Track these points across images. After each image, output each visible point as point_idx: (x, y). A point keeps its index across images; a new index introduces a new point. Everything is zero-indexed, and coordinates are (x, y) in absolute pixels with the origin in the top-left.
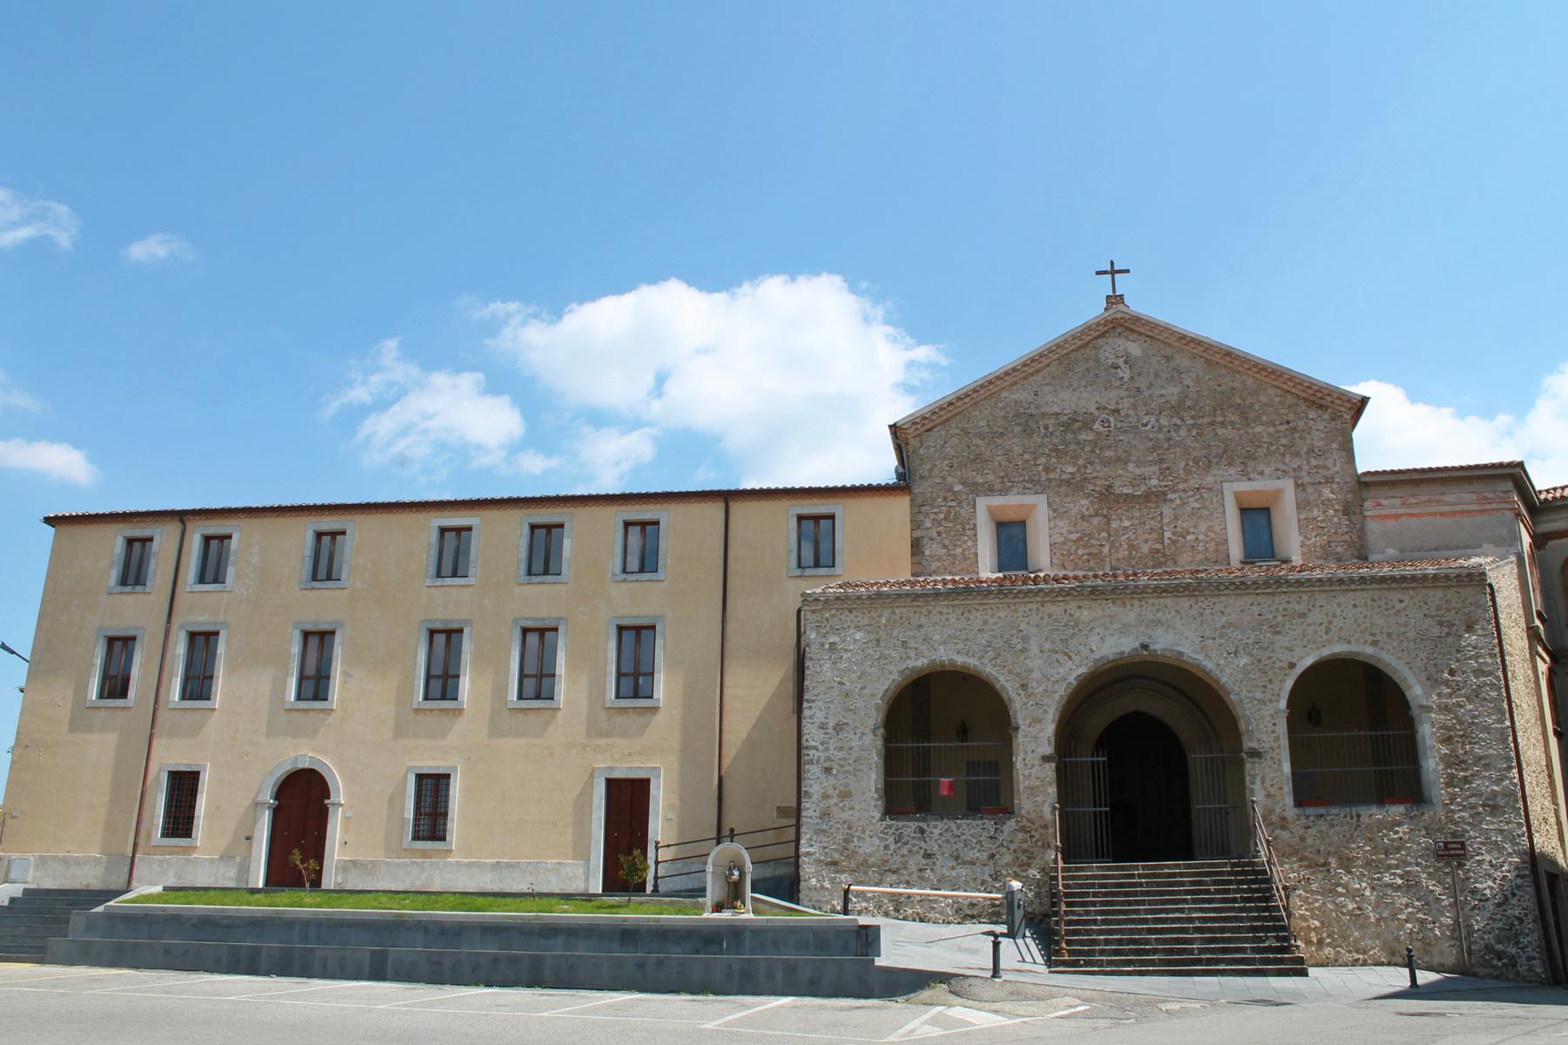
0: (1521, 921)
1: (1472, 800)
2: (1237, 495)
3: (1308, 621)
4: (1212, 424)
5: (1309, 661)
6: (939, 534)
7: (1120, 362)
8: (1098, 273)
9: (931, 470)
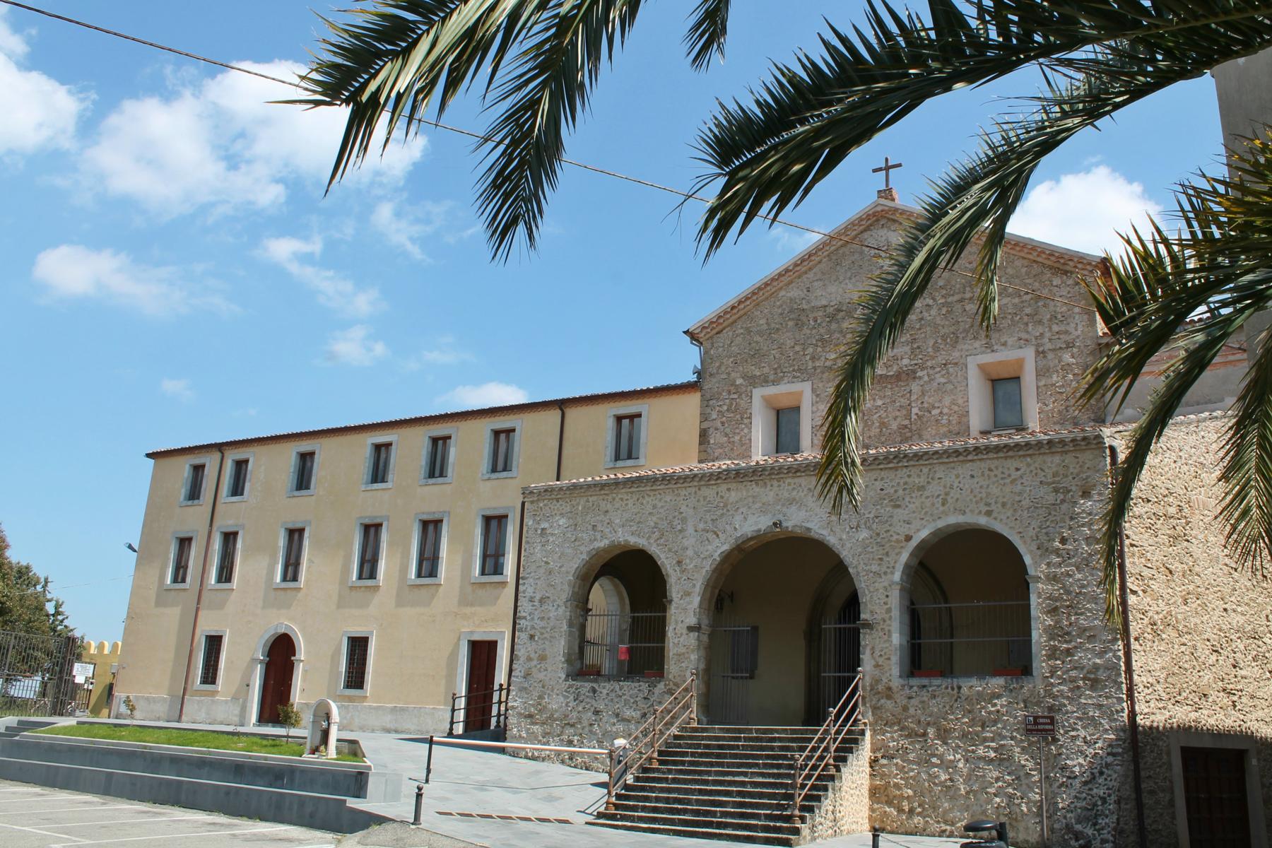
0: (1104, 800)
1: (1073, 673)
2: (982, 368)
3: (926, 493)
4: (961, 301)
5: (924, 534)
6: (723, 423)
8: (900, 165)
9: (719, 367)
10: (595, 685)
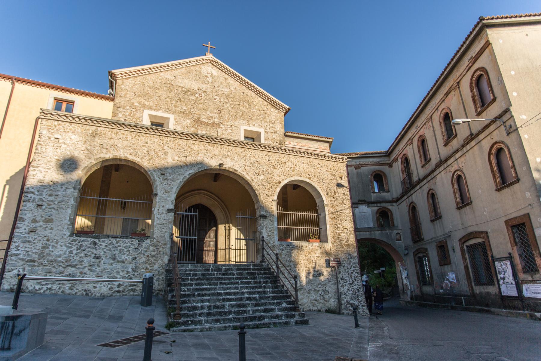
0: (359, 291)
2: (245, 130)
7: (209, 75)
9: (125, 95)
10: (96, 241)
